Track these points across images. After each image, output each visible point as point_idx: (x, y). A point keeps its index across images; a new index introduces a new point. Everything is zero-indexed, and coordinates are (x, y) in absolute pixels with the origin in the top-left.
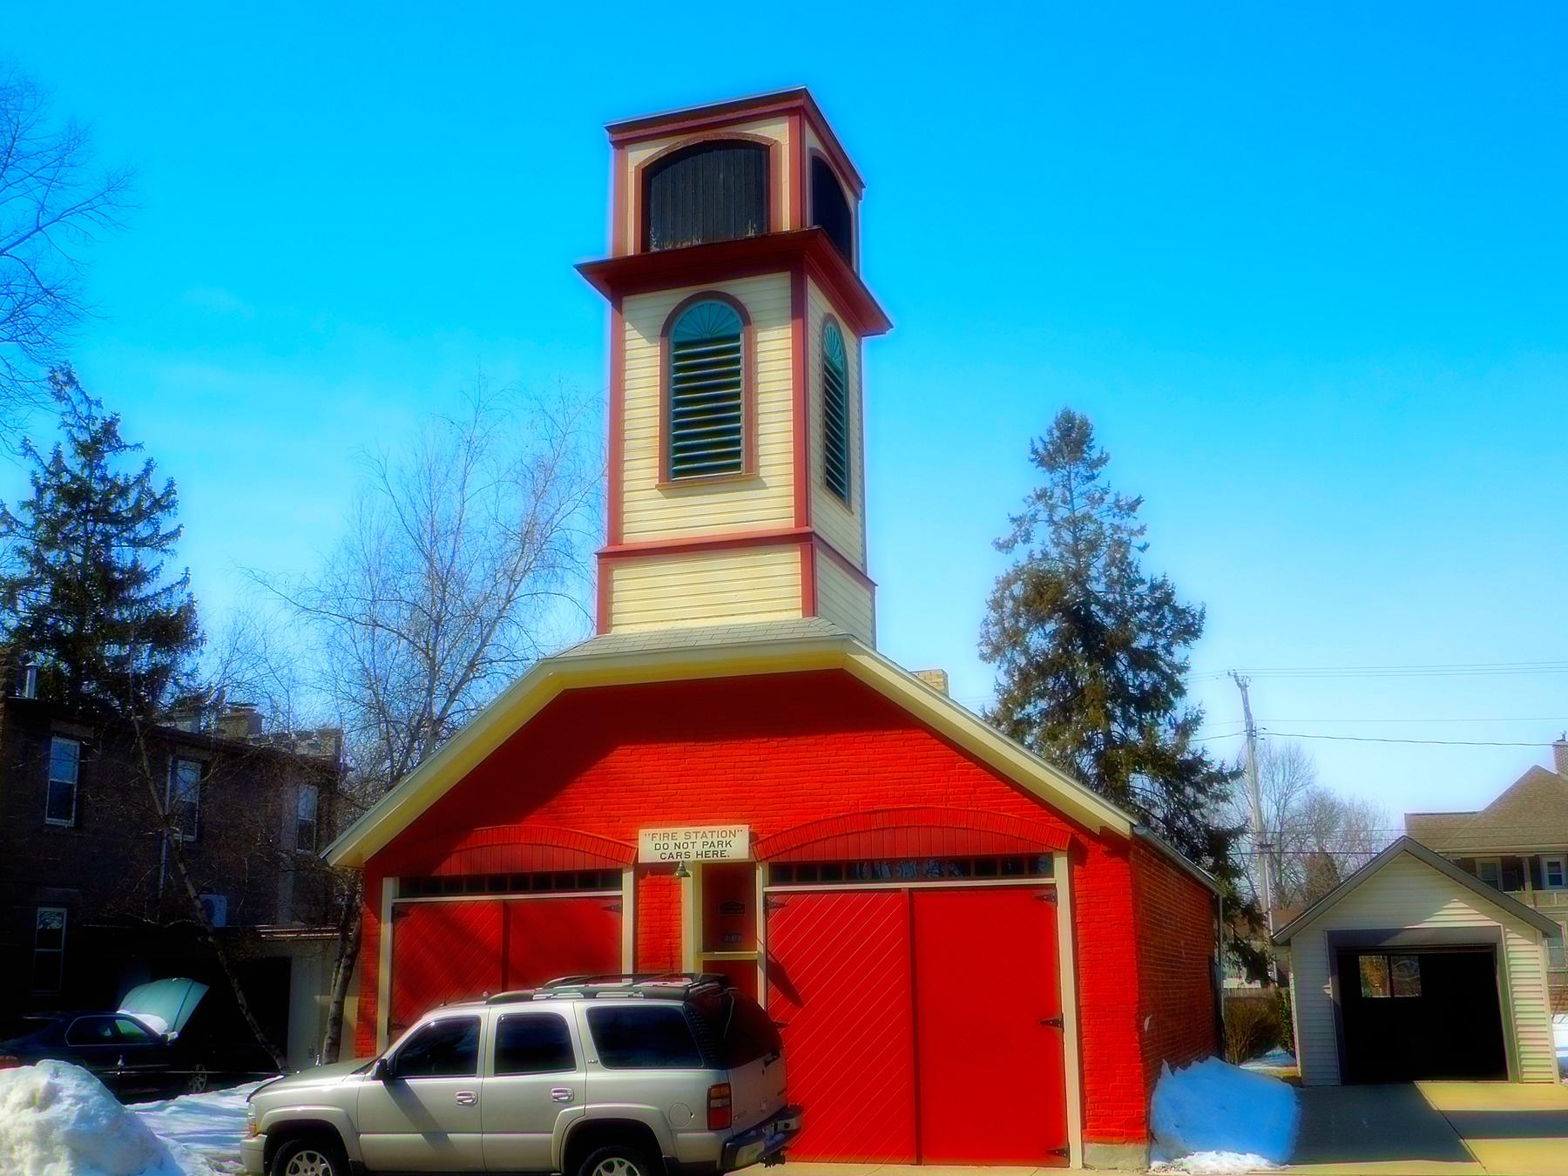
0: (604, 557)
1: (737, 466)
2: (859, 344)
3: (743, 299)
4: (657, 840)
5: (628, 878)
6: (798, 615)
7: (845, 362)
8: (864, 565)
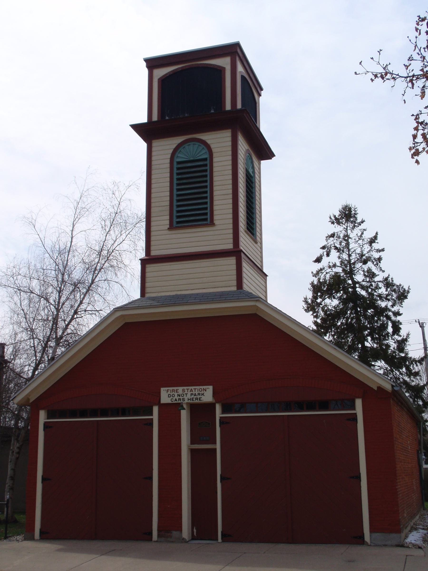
0: (144, 262)
1: (206, 220)
2: (260, 164)
3: (209, 142)
4: (169, 393)
5: (156, 409)
6: (235, 289)
7: (254, 172)
8: (262, 266)
